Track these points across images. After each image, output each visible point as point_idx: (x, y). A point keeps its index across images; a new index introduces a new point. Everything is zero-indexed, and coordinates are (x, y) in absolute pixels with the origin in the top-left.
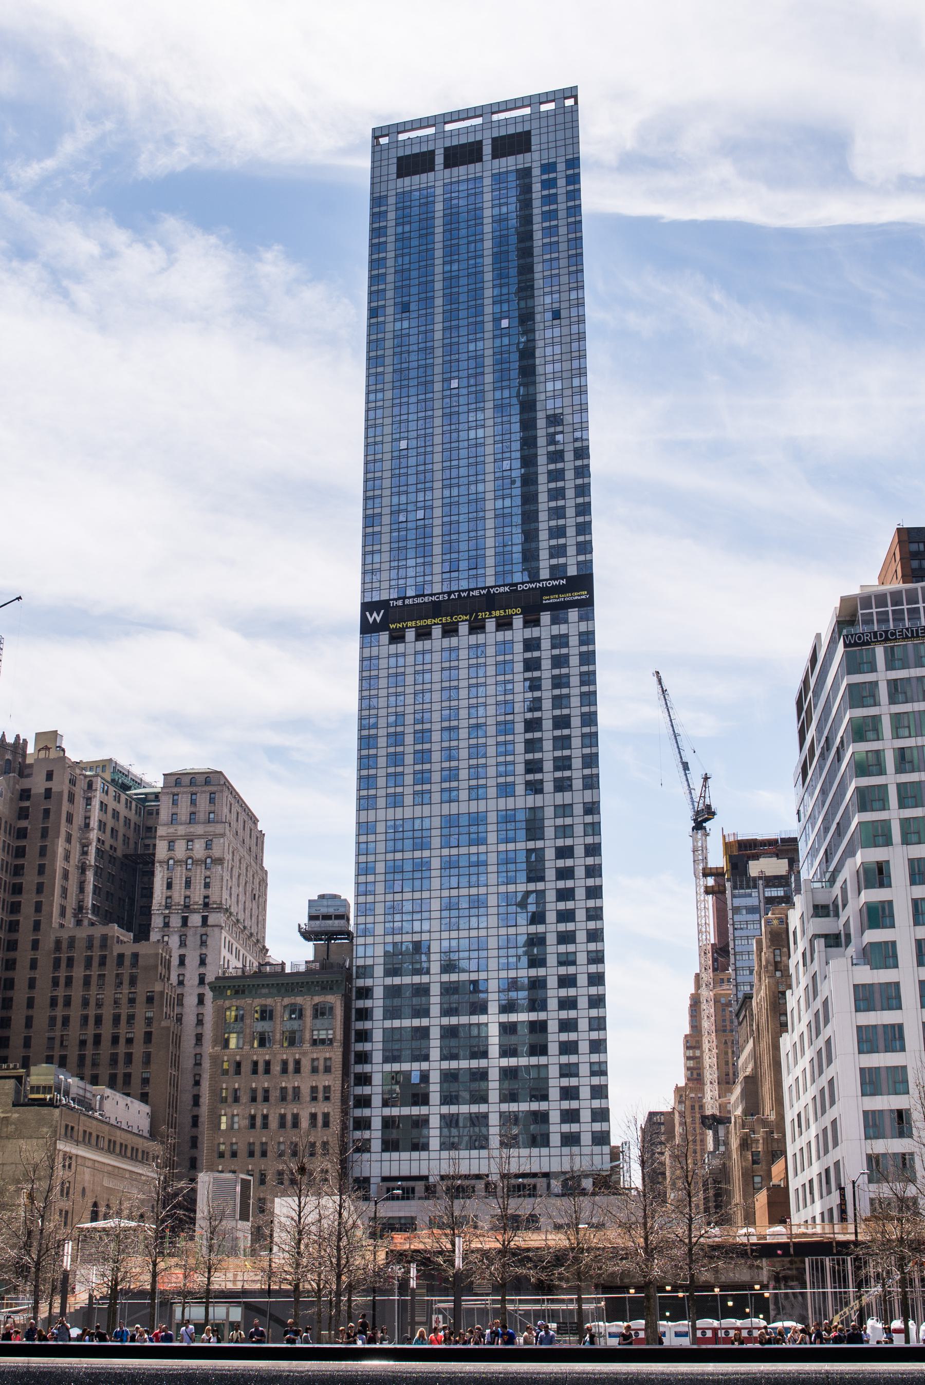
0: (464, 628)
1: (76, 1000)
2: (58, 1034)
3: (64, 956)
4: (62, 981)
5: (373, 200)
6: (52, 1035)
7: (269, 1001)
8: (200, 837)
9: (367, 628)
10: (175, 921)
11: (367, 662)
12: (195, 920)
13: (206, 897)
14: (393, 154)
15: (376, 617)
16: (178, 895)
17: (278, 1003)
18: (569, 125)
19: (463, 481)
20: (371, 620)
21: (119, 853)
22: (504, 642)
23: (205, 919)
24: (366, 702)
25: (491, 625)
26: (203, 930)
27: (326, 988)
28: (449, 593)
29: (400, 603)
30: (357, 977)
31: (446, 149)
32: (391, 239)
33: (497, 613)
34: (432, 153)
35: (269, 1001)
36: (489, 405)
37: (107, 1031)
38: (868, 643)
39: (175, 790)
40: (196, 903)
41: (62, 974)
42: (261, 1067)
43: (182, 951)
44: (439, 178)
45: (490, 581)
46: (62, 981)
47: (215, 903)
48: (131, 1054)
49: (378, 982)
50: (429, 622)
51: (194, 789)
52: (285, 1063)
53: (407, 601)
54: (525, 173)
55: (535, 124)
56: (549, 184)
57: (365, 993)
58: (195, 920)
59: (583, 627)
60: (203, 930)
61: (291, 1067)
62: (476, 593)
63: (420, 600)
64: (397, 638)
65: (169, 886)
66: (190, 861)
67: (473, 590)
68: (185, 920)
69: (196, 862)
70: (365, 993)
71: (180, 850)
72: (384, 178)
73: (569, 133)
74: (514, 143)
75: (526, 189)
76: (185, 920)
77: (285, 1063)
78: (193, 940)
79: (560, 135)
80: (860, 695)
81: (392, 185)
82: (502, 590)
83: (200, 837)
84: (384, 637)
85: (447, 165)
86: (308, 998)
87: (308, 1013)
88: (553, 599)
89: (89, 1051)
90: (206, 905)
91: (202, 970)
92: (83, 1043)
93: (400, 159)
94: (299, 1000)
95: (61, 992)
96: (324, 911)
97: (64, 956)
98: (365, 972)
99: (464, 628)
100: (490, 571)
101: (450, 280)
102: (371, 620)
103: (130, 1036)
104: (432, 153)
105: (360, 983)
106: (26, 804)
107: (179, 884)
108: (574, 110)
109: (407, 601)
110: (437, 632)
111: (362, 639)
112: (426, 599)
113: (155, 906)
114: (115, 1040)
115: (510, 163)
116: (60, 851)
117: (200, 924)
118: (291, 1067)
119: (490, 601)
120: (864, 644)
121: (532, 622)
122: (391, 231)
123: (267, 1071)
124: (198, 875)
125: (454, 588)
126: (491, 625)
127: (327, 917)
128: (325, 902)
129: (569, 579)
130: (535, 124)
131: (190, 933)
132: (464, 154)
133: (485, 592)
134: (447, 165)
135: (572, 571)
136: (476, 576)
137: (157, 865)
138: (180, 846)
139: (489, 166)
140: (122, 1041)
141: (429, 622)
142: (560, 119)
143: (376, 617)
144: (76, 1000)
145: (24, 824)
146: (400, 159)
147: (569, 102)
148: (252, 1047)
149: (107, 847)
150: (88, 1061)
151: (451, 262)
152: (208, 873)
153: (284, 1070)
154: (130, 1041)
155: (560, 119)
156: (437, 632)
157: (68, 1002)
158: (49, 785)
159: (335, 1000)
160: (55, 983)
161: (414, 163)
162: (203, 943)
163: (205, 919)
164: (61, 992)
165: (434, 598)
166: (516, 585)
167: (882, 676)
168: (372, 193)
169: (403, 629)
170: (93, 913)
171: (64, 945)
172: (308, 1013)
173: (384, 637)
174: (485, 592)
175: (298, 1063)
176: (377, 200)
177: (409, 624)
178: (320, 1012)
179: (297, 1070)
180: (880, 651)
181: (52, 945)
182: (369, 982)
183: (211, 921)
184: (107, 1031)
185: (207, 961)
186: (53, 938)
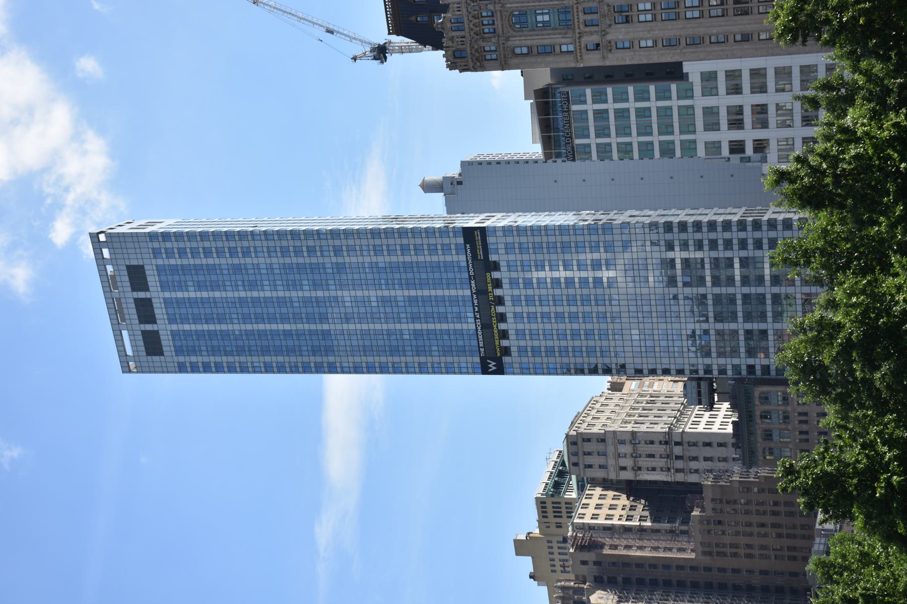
0: (500, 309)
1: (747, 540)
2: (772, 553)
3: (715, 550)
4: (734, 550)
5: (180, 371)
6: (773, 557)
7: (759, 432)
8: (616, 448)
9: (500, 371)
10: (679, 464)
11: (525, 370)
12: (677, 450)
13: (661, 443)
14: (144, 359)
15: (492, 365)
16: (660, 463)
17: (760, 426)
18: (122, 239)
19: (395, 310)
20: (494, 368)
21: (627, 503)
22: (510, 283)
23: (677, 444)
24: (552, 371)
25: (498, 292)
26: (686, 445)
27: (749, 398)
28: (476, 318)
29: (482, 350)
30: (740, 374)
31: (141, 322)
32: (212, 359)
33: (490, 288)
34: (144, 333)
35: (759, 432)
36: (339, 293)
37: (769, 519)
38: (573, 148)
39: (581, 466)
40: (666, 450)
41: (728, 551)
42: (804, 437)
43: (701, 459)
44: (163, 327)
45: (468, 292)
46: (734, 550)
47: (665, 437)
48: (801, 525)
49: (743, 361)
50: (496, 331)
51: (581, 453)
52: (801, 422)
53: (481, 345)
54: (160, 269)
55: (121, 262)
56: (169, 254)
57: (751, 368)
58: (677, 450)
59: (500, 234)
60: (686, 445)
61: (803, 418)
62: (476, 302)
63: (481, 338)
64: (506, 351)
65: (654, 469)
66: (635, 456)
67: (473, 304)
68: (678, 458)
69: (635, 450)
70: (751, 368)
71: (628, 462)
72: (164, 364)
73: (130, 239)
74: (137, 277)
75: (174, 269)
76: (678, 458)
77: (801, 422)
78: (693, 452)
79: (130, 245)
80: (604, 152)
81: (168, 359)
82: (473, 285)
83: (616, 448)
84: (506, 359)
85: (153, 321)
86: (756, 408)
87: (766, 407)
88: (480, 253)
89: (784, 531)
90: (666, 443)
91: (715, 445)
92: (779, 536)
93: (149, 353)
94: (758, 413)
95: (742, 551)
96: (695, 395)
97: (715, 550)
98: (737, 369)
99: (500, 309)
100: (460, 292)
101: (245, 319)
102: (494, 368)
103: (771, 503)
104: (144, 333)
105: (744, 373)
106: (605, 578)
107: (651, 463)
108: (109, 236)
109: (481, 345)
110: (503, 326)
111: (507, 374)
112: (480, 333)
113: (669, 479)
114: (775, 513)
115: (152, 280)
116: (639, 553)
117: (680, 447)
118: (803, 418)
119: (481, 292)
120: (573, 150)
121: (496, 266)
122: (206, 359)
123: (807, 433)
124: (644, 449)
125: (472, 315)
126: (498, 292)
127: (699, 394)
128: (689, 395)
129: (466, 242)
130: (121, 262)
131: (688, 454)
132: (145, 311)
133: (475, 296)
134: (153, 321)
135: (461, 240)
136: (464, 301)
137: (638, 478)
138: (623, 462)
139: (156, 294)
140: (776, 509)
141: (496, 331)
142: (116, 245)
143: (492, 365)
144: (747, 540)
145: (620, 579)
146: (149, 353)
147: (102, 238)
148: (790, 442)
149: (623, 513)
150: (791, 532)
151: (231, 319)
152: (643, 442)
153: (806, 422)
154: (776, 504)
155: (117, 245)
156: (503, 326)
157: (749, 546)
158: (591, 563)
159: (758, 391)
160: (735, 555)
161: (152, 344)
162: (695, 444)
163: (677, 444)
164: (742, 551)
165: (479, 328)
166: (470, 276)
167: (593, 141)
168: (176, 372)
169: (501, 347)
170: (674, 522)
171: (707, 549)
172: (766, 407)
173: (506, 359)
174: (475, 296)
175: (800, 414)
176: (182, 368)
177: (497, 343)
178: (765, 399)
179: (806, 414)
180: (577, 141)
181: (708, 558)
182: (744, 367)
183: (679, 440)
184: (769, 519)
185: (708, 441)
186: (703, 558)
